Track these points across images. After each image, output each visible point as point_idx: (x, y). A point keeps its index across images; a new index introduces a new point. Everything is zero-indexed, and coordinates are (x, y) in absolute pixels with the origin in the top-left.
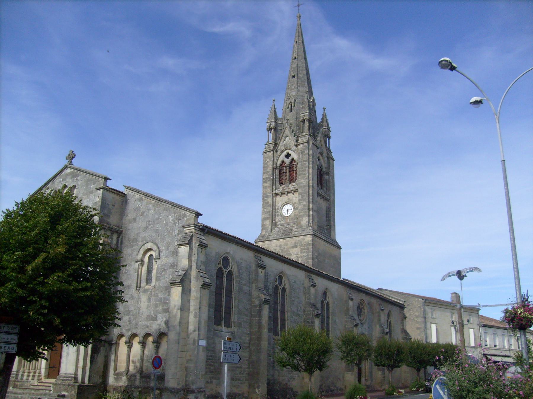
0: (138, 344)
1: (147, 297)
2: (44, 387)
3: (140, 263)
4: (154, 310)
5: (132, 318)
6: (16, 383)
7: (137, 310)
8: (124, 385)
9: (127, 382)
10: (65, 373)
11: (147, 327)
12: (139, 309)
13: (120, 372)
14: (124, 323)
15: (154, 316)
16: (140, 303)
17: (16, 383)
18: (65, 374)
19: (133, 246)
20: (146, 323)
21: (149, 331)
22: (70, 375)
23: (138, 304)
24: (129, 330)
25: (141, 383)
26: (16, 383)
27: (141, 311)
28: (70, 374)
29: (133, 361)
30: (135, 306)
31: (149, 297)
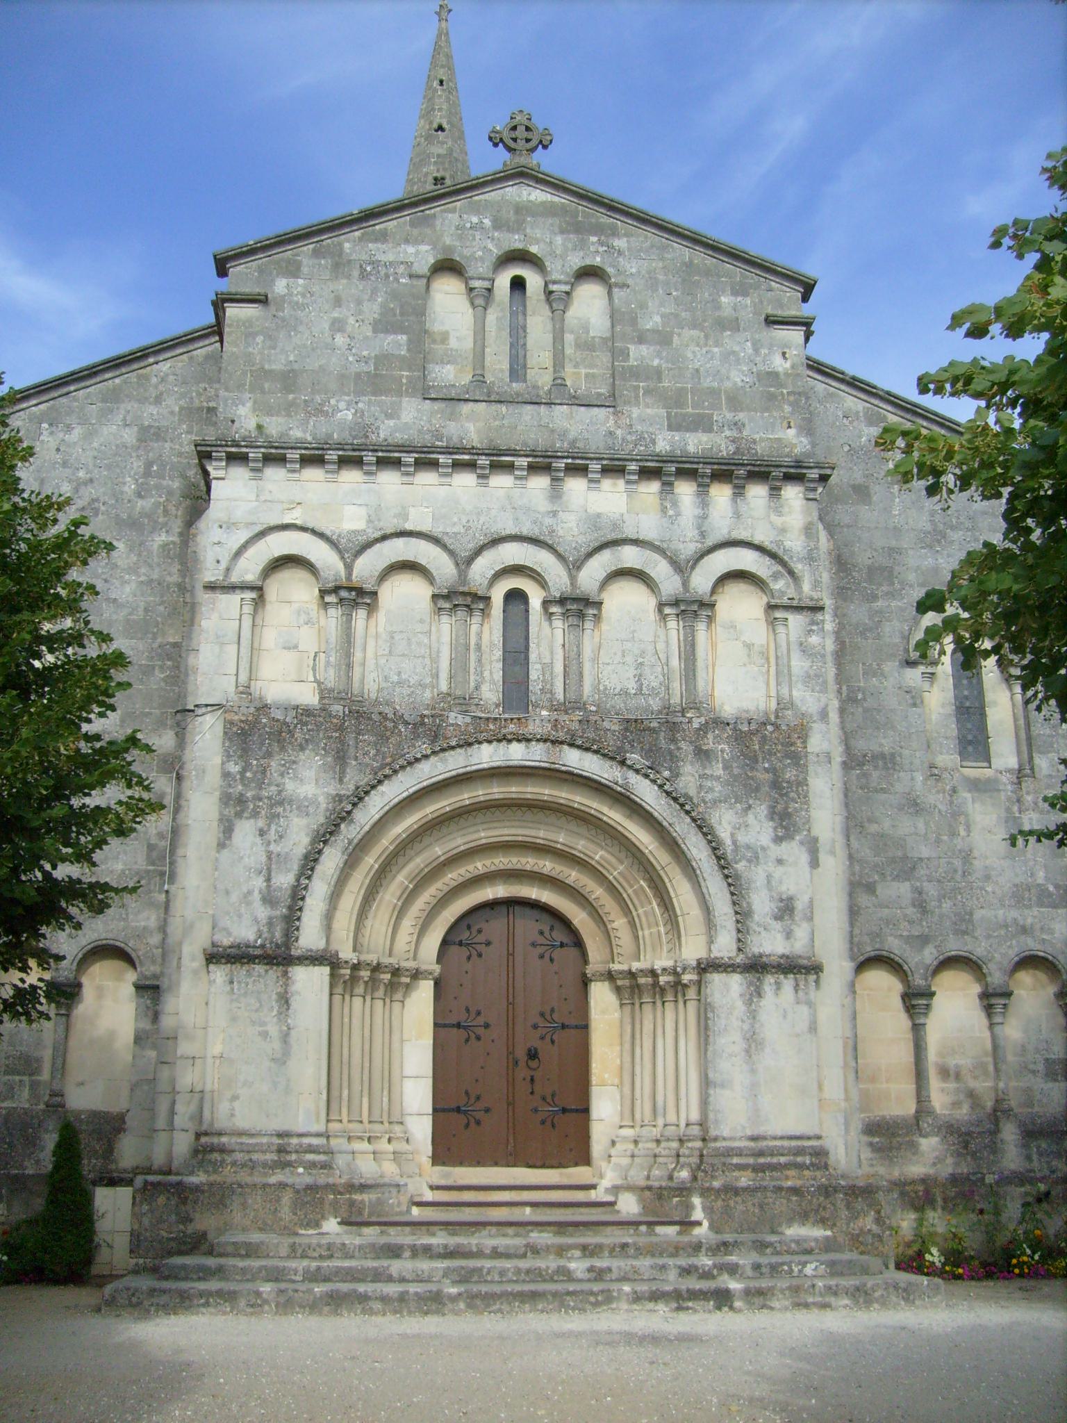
0: (134, 989)
1: (1003, 814)
2: (528, 1210)
3: (253, 595)
4: (1045, 866)
5: (931, 890)
6: (355, 1197)
7: (957, 863)
8: (931, 1171)
9: (950, 1160)
10: (749, 1133)
11: (1024, 930)
12: (967, 856)
13: (884, 1117)
14: (886, 911)
15: (1051, 888)
16: (963, 833)
17: (357, 1197)
18: (754, 1138)
19: (874, 598)
20: (1014, 914)
21: (1039, 947)
22: (799, 1143)
23: (953, 834)
24: (924, 940)
25: (1029, 1158)
26: (355, 1197)
27: (977, 864)
28: (791, 1138)
29: (944, 1073)
30: (938, 841)
31: (1008, 810)
